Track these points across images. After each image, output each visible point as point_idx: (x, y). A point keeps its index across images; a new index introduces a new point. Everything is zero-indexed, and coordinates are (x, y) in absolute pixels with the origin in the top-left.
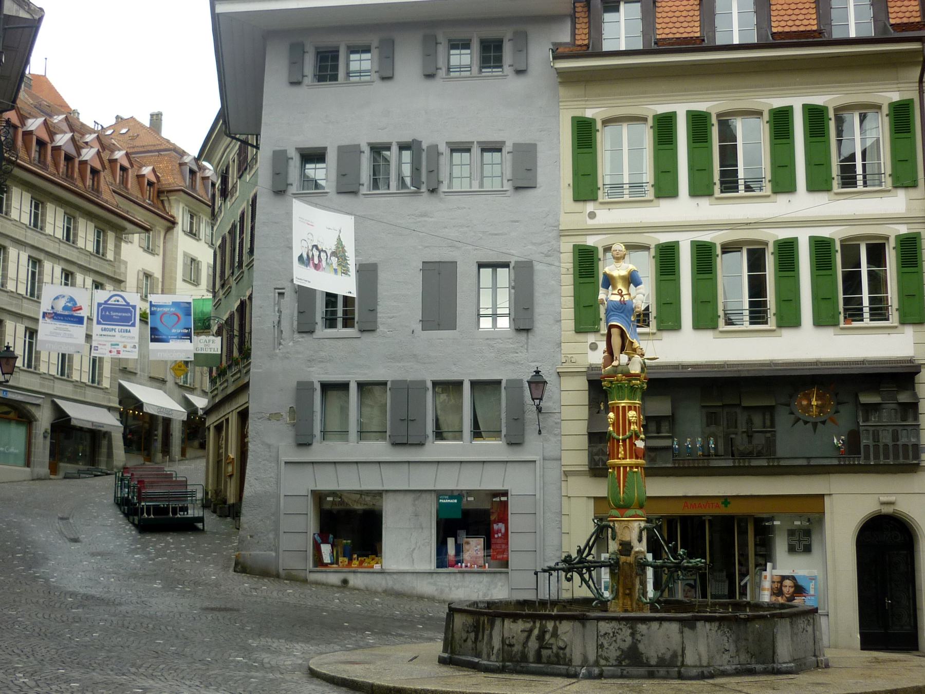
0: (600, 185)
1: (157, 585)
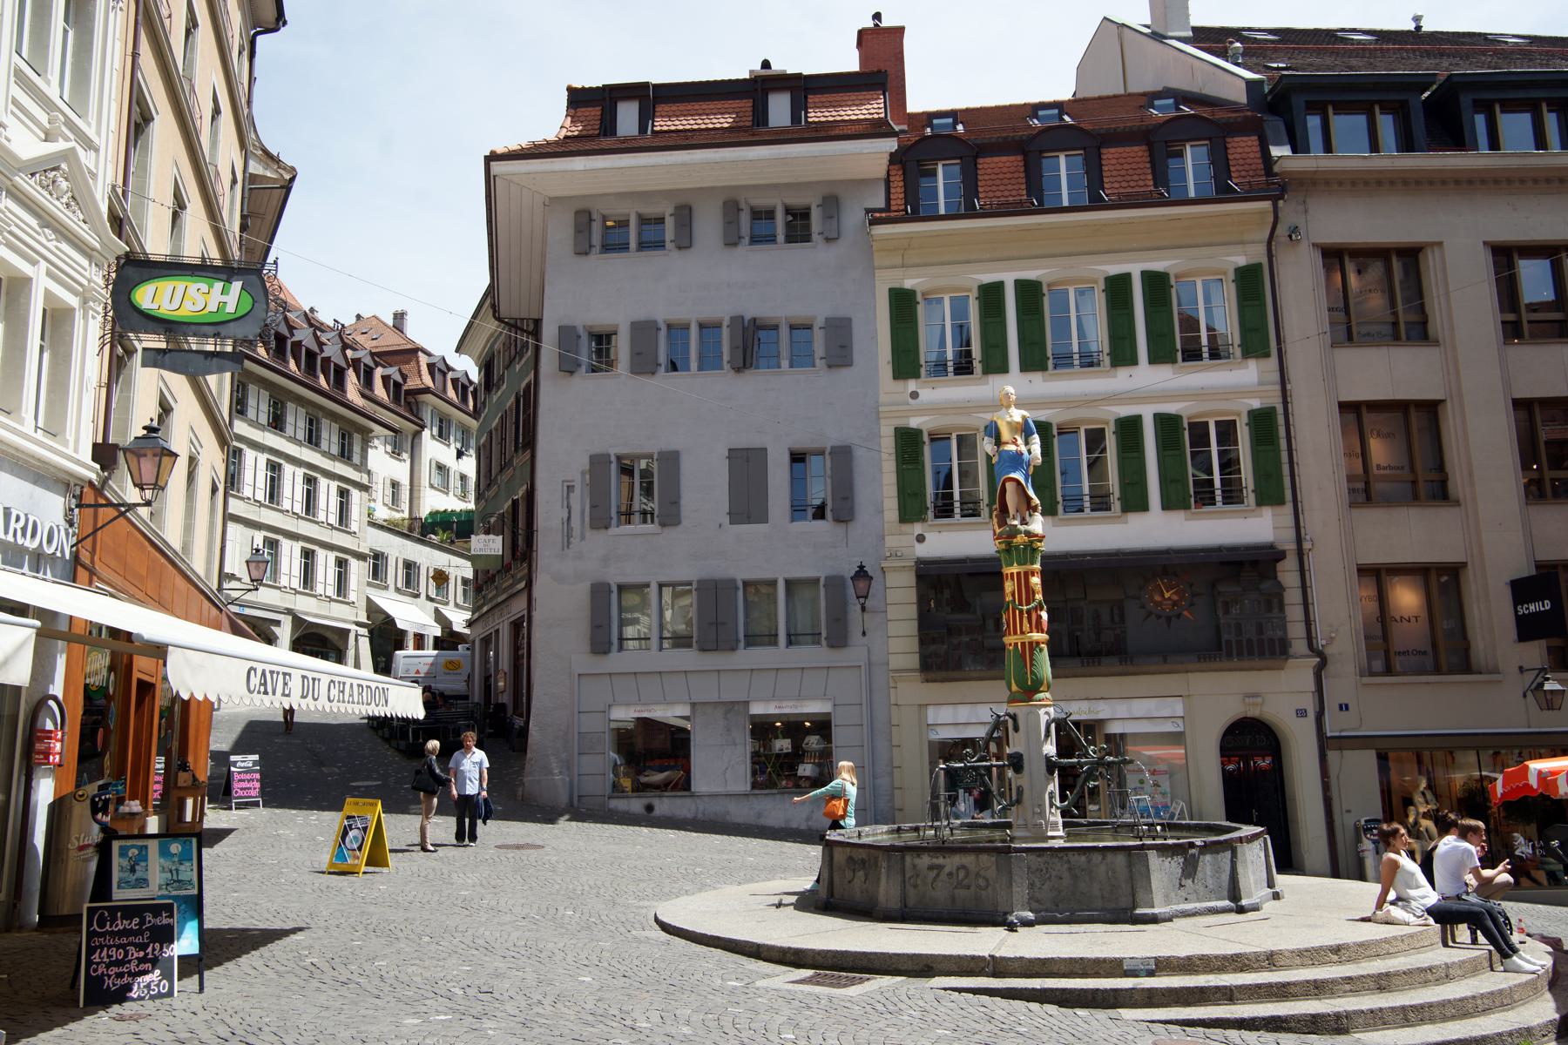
0: (922, 362)
1: (564, 756)
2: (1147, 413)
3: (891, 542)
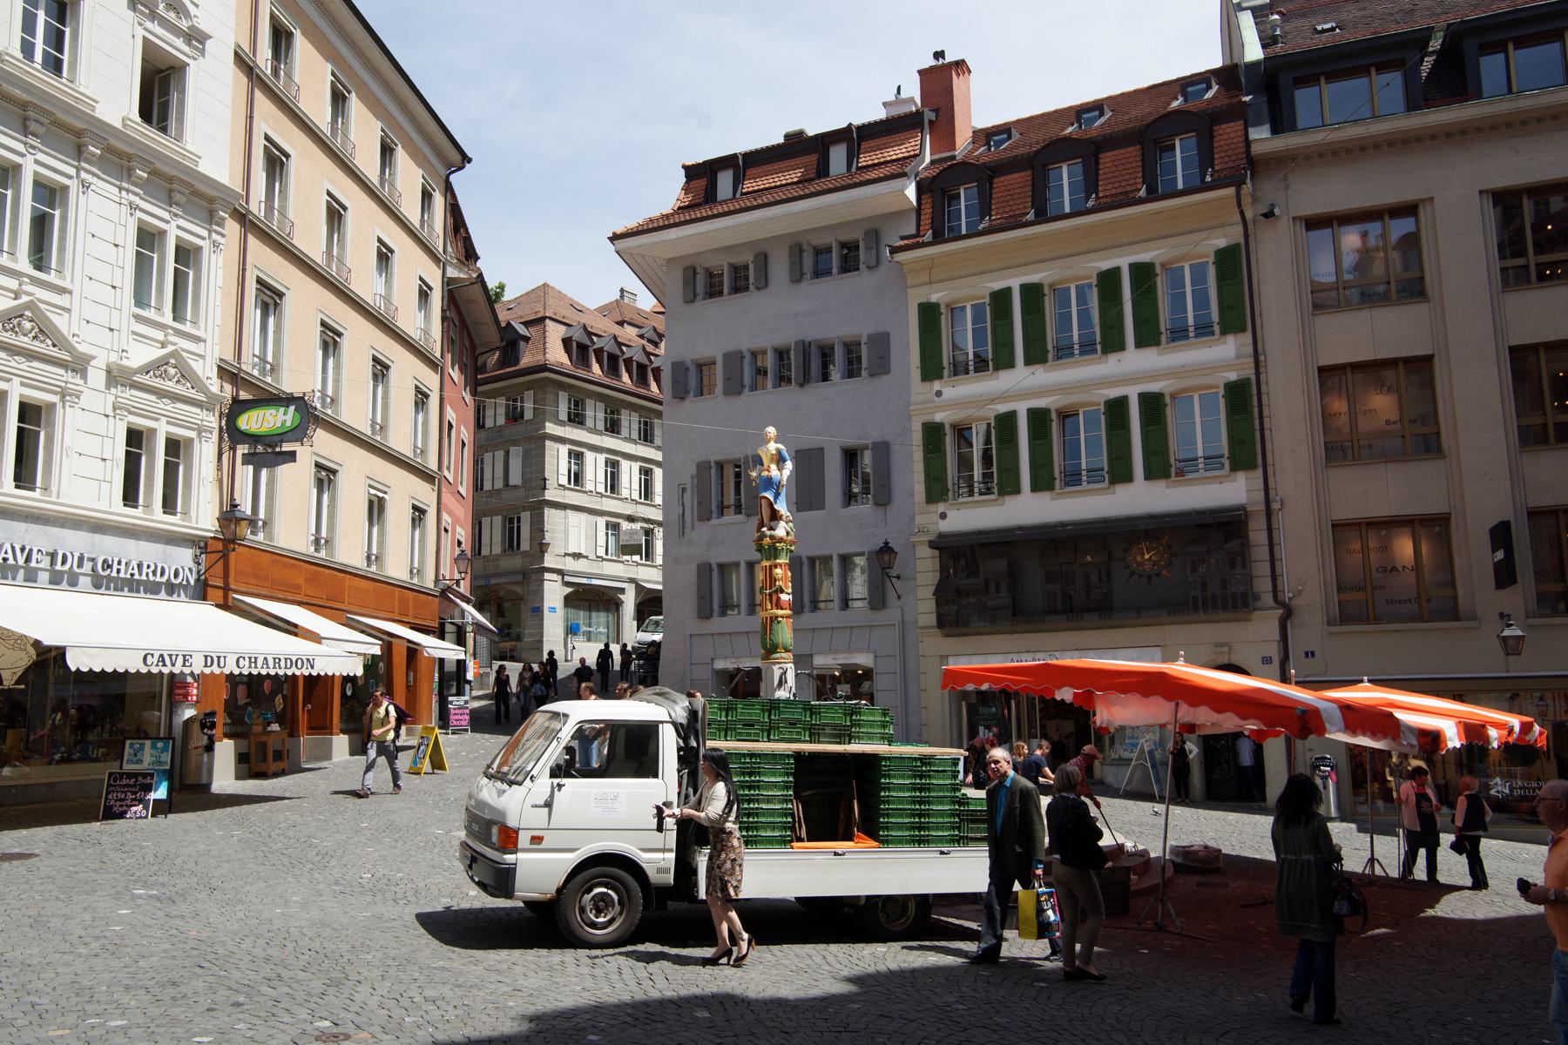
2: (1022, 408)
3: (920, 520)
